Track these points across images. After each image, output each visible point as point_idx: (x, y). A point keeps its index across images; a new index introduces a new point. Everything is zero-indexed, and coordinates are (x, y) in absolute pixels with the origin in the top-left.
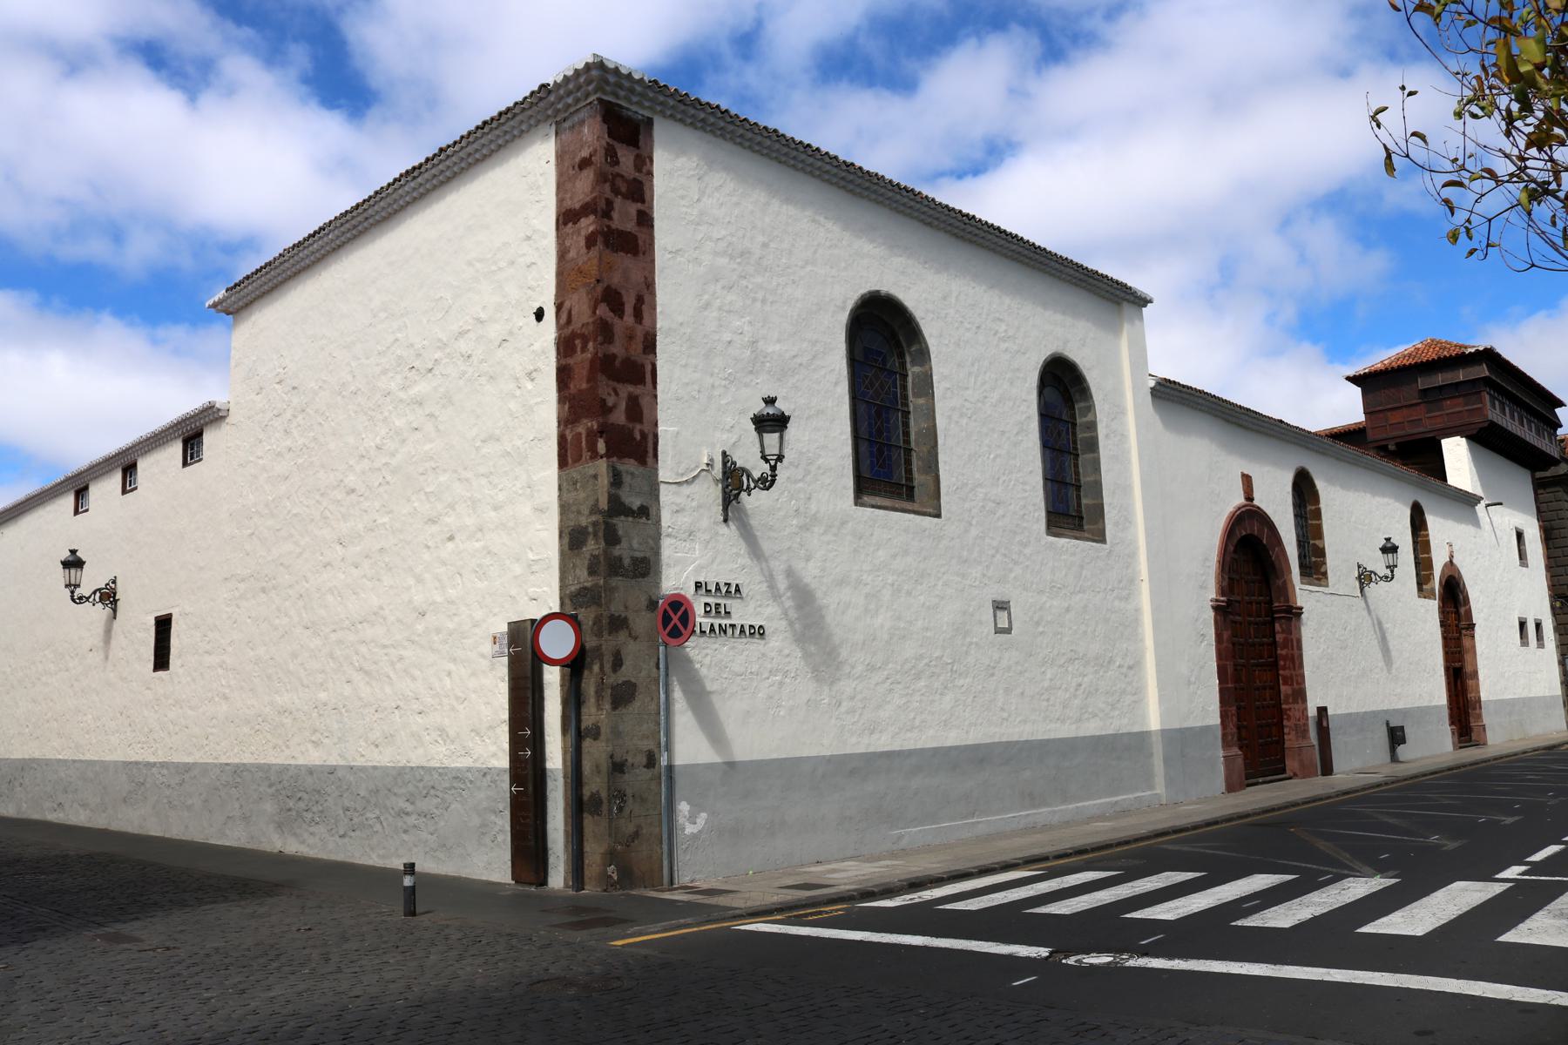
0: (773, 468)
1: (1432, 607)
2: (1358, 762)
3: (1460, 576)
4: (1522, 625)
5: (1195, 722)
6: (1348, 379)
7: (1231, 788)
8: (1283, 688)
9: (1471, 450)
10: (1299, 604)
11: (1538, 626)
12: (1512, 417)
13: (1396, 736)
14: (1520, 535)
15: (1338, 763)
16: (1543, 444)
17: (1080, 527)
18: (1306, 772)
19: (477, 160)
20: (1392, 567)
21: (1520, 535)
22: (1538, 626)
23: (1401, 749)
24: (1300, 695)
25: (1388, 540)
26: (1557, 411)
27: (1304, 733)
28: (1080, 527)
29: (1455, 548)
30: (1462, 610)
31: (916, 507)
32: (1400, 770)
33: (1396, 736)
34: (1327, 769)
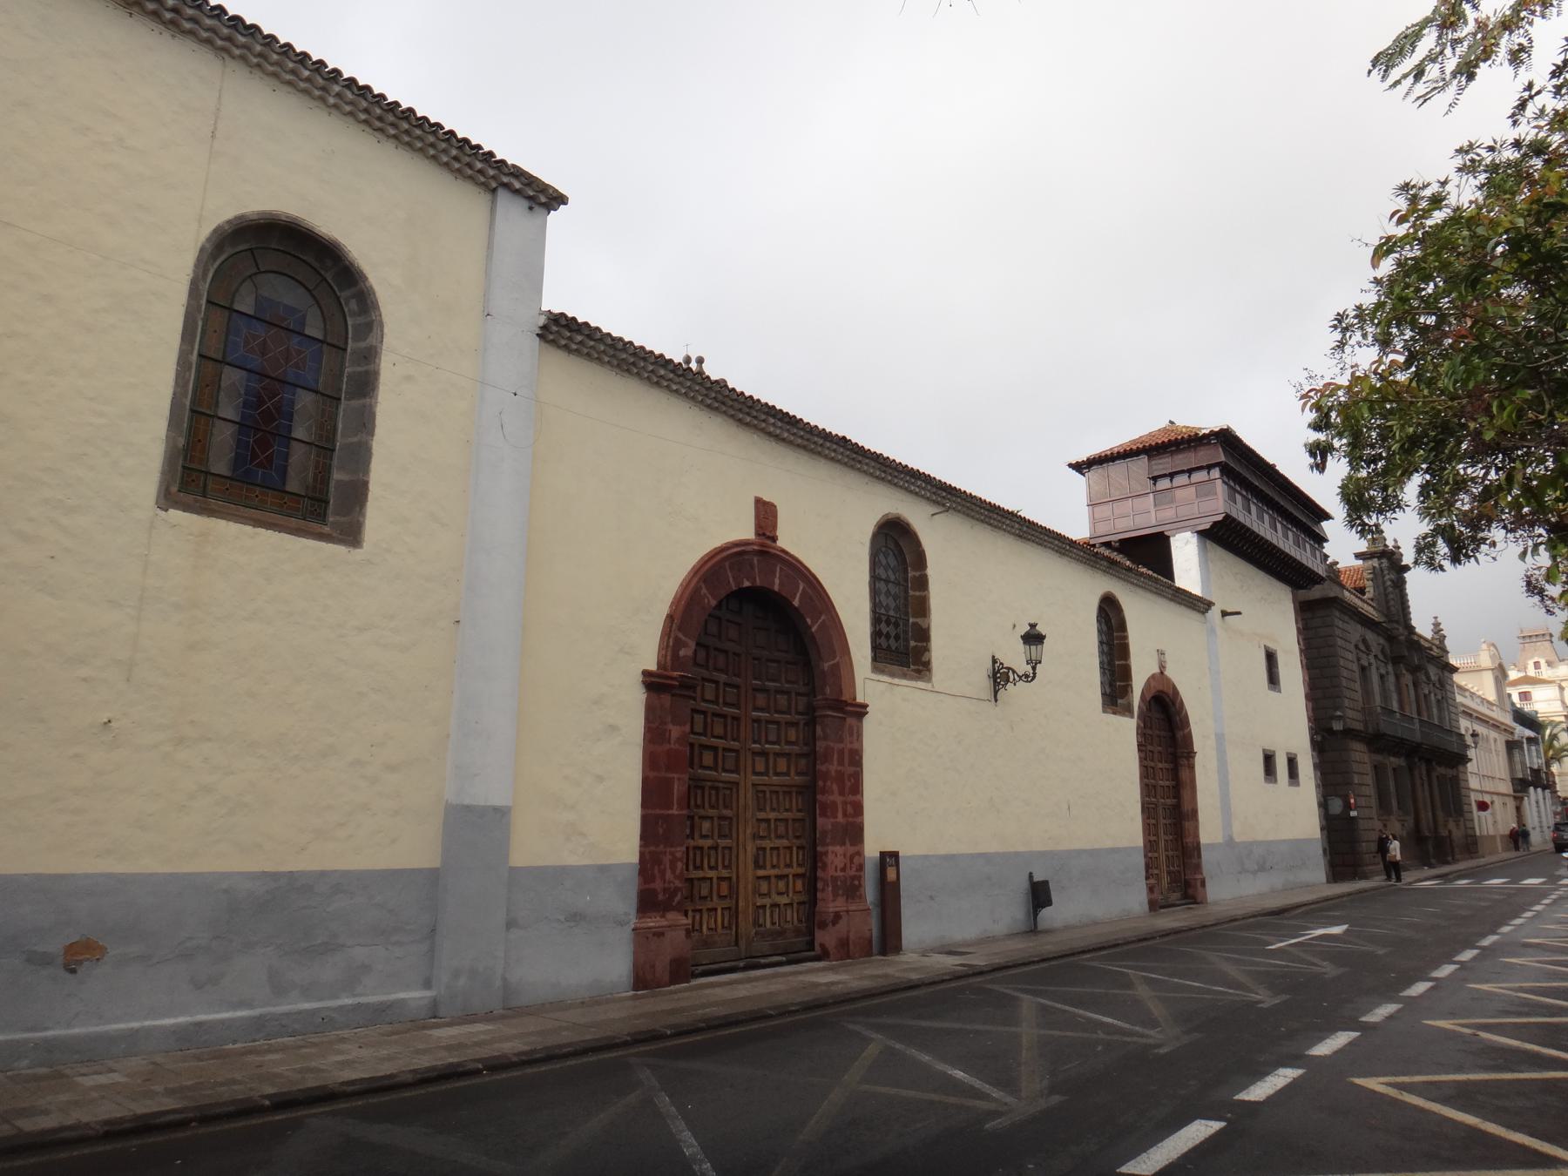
0: (1034, 668)
1: (1125, 730)
2: (934, 931)
3: (1176, 692)
4: (1269, 759)
5: (1124, 843)
6: (1070, 465)
7: (1154, 906)
8: (820, 821)
9: (1203, 551)
10: (860, 699)
11: (1292, 762)
12: (1261, 518)
13: (1039, 895)
14: (1271, 658)
15: (914, 930)
16: (1304, 556)
17: (321, 517)
18: (846, 951)
19: (740, 421)
20: (1034, 663)
21: (1271, 658)
22: (1292, 762)
23: (1045, 912)
24: (854, 833)
25: (1033, 626)
26: (1324, 524)
27: (852, 889)
28: (321, 517)
29: (1167, 658)
30: (1179, 735)
31: (327, 529)
32: (1046, 945)
33: (1039, 895)
34: (890, 940)
